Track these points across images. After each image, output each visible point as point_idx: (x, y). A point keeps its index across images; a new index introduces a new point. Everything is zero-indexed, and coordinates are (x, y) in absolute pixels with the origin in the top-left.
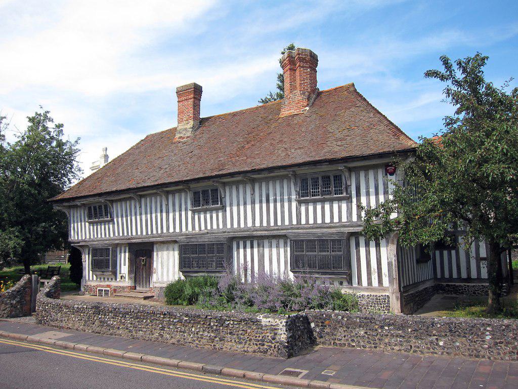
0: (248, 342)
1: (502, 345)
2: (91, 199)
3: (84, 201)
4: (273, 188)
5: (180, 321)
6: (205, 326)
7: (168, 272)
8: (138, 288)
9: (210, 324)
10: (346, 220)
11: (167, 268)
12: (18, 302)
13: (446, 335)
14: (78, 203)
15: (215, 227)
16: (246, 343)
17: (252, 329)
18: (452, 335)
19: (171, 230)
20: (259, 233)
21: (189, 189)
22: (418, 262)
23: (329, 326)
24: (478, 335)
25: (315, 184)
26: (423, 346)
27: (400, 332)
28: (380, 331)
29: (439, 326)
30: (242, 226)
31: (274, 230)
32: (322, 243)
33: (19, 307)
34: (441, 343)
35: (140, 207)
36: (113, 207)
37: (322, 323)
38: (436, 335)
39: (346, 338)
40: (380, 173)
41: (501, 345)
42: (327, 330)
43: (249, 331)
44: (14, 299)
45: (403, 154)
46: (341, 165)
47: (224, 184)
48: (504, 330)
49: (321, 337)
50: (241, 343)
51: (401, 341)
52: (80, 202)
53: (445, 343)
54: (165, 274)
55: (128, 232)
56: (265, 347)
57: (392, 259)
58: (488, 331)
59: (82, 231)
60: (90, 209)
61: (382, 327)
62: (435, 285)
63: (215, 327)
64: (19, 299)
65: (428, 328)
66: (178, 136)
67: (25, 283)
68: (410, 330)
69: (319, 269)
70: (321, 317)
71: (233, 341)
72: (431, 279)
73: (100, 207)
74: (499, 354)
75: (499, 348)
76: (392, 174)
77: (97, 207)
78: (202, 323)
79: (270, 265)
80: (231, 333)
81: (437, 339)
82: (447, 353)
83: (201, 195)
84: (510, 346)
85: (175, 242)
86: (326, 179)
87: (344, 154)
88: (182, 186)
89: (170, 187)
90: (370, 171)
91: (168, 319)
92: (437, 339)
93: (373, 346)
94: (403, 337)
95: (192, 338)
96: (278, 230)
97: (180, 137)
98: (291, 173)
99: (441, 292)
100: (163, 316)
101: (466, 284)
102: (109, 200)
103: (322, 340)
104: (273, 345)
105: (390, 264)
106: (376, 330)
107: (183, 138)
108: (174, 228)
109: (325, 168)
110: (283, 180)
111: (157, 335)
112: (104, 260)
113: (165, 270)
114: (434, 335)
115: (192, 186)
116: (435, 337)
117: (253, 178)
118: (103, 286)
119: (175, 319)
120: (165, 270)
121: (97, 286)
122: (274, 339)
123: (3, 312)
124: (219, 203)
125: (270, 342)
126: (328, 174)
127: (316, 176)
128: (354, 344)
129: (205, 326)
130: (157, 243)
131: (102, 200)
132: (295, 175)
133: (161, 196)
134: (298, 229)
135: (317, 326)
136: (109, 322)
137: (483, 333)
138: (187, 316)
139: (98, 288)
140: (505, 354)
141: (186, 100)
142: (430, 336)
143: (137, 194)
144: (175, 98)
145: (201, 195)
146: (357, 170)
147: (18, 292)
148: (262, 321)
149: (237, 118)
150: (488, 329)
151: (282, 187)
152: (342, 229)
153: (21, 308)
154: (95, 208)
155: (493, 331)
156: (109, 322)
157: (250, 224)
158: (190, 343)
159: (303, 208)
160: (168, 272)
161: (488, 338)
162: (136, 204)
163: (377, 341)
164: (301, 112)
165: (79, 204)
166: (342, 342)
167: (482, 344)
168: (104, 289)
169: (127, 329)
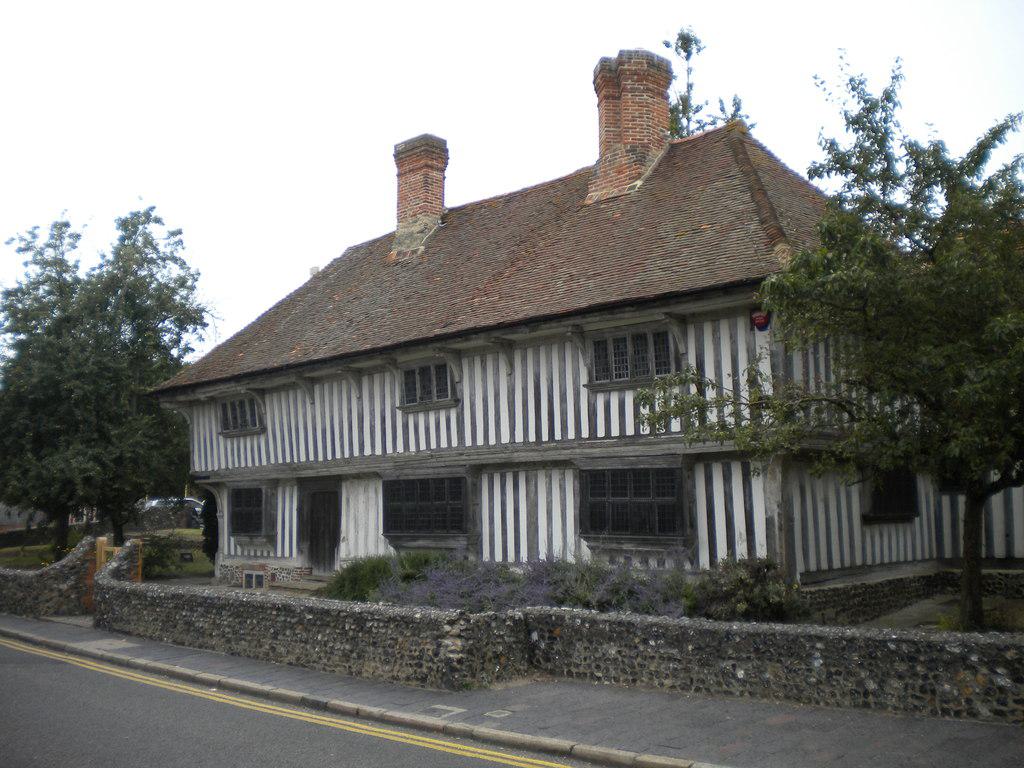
0: (399, 662)
2: (223, 388)
3: (212, 391)
4: (547, 363)
5: (300, 622)
6: (338, 631)
7: (366, 536)
8: (316, 572)
9: (344, 628)
10: (678, 429)
12: (73, 588)
13: (749, 658)
14: (201, 395)
15: (444, 444)
16: (395, 661)
17: (405, 636)
18: (759, 659)
19: (368, 452)
21: (394, 364)
22: (867, 520)
23: (561, 637)
24: (801, 658)
26: (712, 679)
28: (641, 648)
29: (738, 640)
30: (492, 441)
31: (550, 449)
33: (73, 596)
34: (740, 674)
35: (313, 403)
36: (264, 403)
37: (550, 632)
38: (732, 658)
39: (588, 661)
40: (742, 325)
41: (838, 677)
42: (558, 647)
43: (400, 640)
44: (64, 582)
45: (377, 362)
46: (657, 311)
47: (459, 355)
48: (844, 649)
49: (548, 660)
50: (387, 662)
51: (676, 669)
52: (204, 393)
53: (746, 674)
54: (361, 542)
55: (292, 456)
56: (425, 670)
57: (773, 511)
58: (817, 649)
59: (214, 452)
60: (224, 407)
61: (645, 642)
62: (936, 575)
63: (351, 633)
64: (73, 582)
65: (720, 643)
67: (86, 553)
68: (690, 648)
71: (377, 659)
72: (924, 560)
73: (242, 403)
74: (833, 695)
75: (834, 683)
76: (762, 327)
78: (332, 624)
79: (548, 525)
80: (374, 644)
82: (750, 693)
83: (418, 377)
84: (852, 679)
85: (376, 475)
87: (665, 288)
88: (382, 358)
91: (283, 619)
94: (680, 661)
95: (318, 653)
96: (556, 449)
98: (570, 329)
99: (949, 588)
101: (1000, 571)
103: (549, 666)
104: (435, 668)
105: (769, 522)
106: (636, 647)
107: (405, 254)
108: (343, 453)
109: (628, 318)
110: (526, 349)
112: (252, 513)
113: (362, 534)
114: (730, 658)
115: (402, 358)
116: (731, 662)
117: (506, 339)
118: (252, 568)
119: (293, 617)
120: (362, 534)
121: (243, 567)
122: (436, 654)
123: (47, 605)
124: (673, 369)
125: (431, 660)
126: (641, 330)
127: (620, 334)
128: (600, 675)
129: (338, 631)
131: (241, 389)
132: (580, 333)
133: (347, 379)
134: (592, 446)
135: (542, 637)
136: (197, 624)
137: (810, 655)
139: (246, 572)
140: (843, 695)
142: (724, 659)
143: (305, 375)
144: (392, 169)
145: (418, 377)
146: (697, 319)
147: (72, 568)
149: (514, 205)
151: (563, 360)
152: (672, 445)
153: (78, 599)
154: (233, 404)
155: (826, 650)
156: (197, 624)
157: (505, 439)
160: (366, 536)
161: (817, 663)
163: (638, 669)
164: (626, 192)
165: (202, 397)
166: (581, 669)
167: (807, 676)
168: (255, 573)
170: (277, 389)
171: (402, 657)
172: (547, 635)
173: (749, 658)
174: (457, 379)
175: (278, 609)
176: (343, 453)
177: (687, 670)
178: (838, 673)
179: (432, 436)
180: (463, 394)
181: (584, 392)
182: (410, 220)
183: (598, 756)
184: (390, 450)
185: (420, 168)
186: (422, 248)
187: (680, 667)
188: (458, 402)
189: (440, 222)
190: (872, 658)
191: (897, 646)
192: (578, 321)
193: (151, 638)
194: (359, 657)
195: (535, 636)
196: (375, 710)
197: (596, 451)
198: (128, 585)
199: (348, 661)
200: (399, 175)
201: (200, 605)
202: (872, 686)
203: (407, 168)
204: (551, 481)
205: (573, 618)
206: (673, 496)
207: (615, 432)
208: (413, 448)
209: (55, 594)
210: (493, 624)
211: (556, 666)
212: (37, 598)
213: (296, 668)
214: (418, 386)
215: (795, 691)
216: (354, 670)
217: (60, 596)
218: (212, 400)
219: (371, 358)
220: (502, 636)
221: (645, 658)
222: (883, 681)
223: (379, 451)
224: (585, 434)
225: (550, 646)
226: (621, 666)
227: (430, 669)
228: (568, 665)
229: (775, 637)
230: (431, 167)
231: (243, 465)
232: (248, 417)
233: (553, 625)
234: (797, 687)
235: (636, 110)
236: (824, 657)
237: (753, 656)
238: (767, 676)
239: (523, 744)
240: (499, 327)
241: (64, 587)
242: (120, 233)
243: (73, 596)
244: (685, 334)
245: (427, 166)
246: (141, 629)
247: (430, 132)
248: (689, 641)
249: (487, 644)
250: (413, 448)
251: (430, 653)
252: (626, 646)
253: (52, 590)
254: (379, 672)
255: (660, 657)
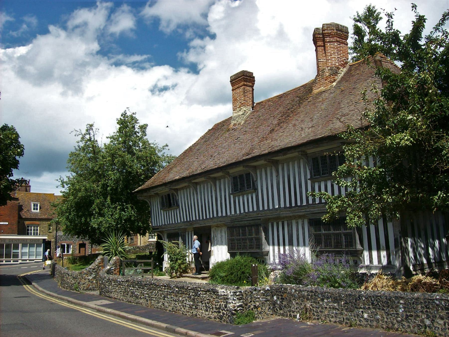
1: (413, 318)
9: (189, 295)
12: (94, 278)
13: (369, 308)
18: (373, 308)
19: (220, 214)
27: (335, 305)
29: (364, 299)
34: (366, 315)
36: (178, 195)
44: (91, 275)
49: (281, 309)
50: (207, 311)
51: (336, 313)
52: (153, 192)
55: (159, 223)
58: (401, 303)
61: (322, 300)
66: (233, 122)
69: (335, 248)
70: (280, 290)
74: (409, 327)
75: (410, 321)
81: (362, 312)
82: (370, 325)
83: (238, 179)
84: (418, 319)
92: (362, 312)
93: (317, 317)
94: (338, 309)
97: (235, 125)
102: (174, 189)
103: (282, 312)
104: (225, 313)
106: (319, 303)
108: (279, 204)
115: (231, 171)
116: (361, 310)
135: (278, 298)
138: (177, 287)
145: (238, 179)
148: (219, 291)
150: (401, 302)
155: (405, 304)
165: (153, 194)
169: (145, 299)
170: (182, 188)
171: (213, 308)
172: (280, 297)
173: (369, 308)
174: (255, 180)
175: (165, 286)
176: (279, 204)
177: (342, 314)
178: (411, 316)
179: (246, 205)
180: (258, 186)
181: (309, 182)
182: (238, 109)
184: (229, 214)
185: (241, 86)
186: (243, 122)
187: (338, 312)
188: (256, 190)
189: (251, 109)
190: (427, 308)
191: (440, 302)
192: (303, 149)
194: (196, 308)
195: (275, 298)
198: (111, 277)
199: (191, 310)
200: (233, 90)
201: (137, 285)
202: (428, 322)
203: (236, 87)
204: (298, 224)
205: (291, 289)
208: (238, 212)
210: (254, 292)
211: (284, 312)
212: (79, 283)
214: (239, 183)
215: (391, 325)
216: (194, 314)
219: (218, 172)
220: (259, 298)
221: (322, 308)
222: (433, 320)
223: (224, 214)
225: (281, 302)
226: (312, 312)
227: (223, 313)
228: (290, 311)
229: (381, 297)
230: (246, 85)
231: (251, 210)
232: (172, 201)
233: (283, 293)
234: (392, 323)
235: (332, 51)
236: (404, 308)
237: (371, 307)
238: (378, 317)
240: (270, 153)
241: (90, 278)
242: (118, 126)
243: (94, 282)
244: (256, 173)
245: (244, 85)
246: (116, 295)
247: (245, 69)
248: (341, 300)
249: (251, 302)
250: (238, 212)
251: (223, 306)
252: (314, 302)
253: (85, 279)
254: (204, 315)
255: (330, 308)
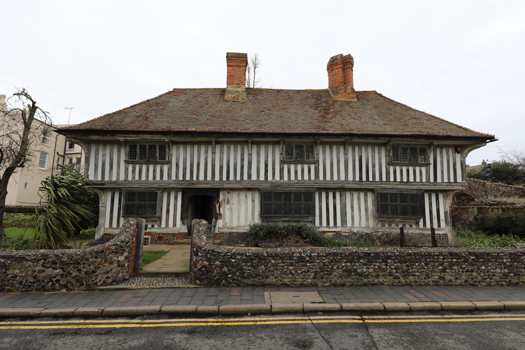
11: (239, 214)
20: (350, 186)
25: (405, 150)
32: (403, 196)
40: (451, 151)
44: (122, 254)
52: (124, 137)
60: (131, 147)
76: (458, 153)
77: (147, 146)
85: (257, 189)
86: (414, 149)
89: (267, 137)
90: (262, 146)
100: (442, 257)
105: (446, 213)
111: (437, 277)
123: (107, 275)
130: (224, 189)
141: (238, 66)
158: (480, 281)
159: (286, 167)
162: (207, 149)
183: (129, 313)
193: (437, 284)
196: (402, 305)
197: (388, 186)
206: (417, 203)
207: (398, 179)
209: (115, 265)
213: (495, 287)
217: (119, 266)
218: (126, 142)
224: (384, 179)
239: (334, 309)
241: (121, 258)
250: (321, 178)
